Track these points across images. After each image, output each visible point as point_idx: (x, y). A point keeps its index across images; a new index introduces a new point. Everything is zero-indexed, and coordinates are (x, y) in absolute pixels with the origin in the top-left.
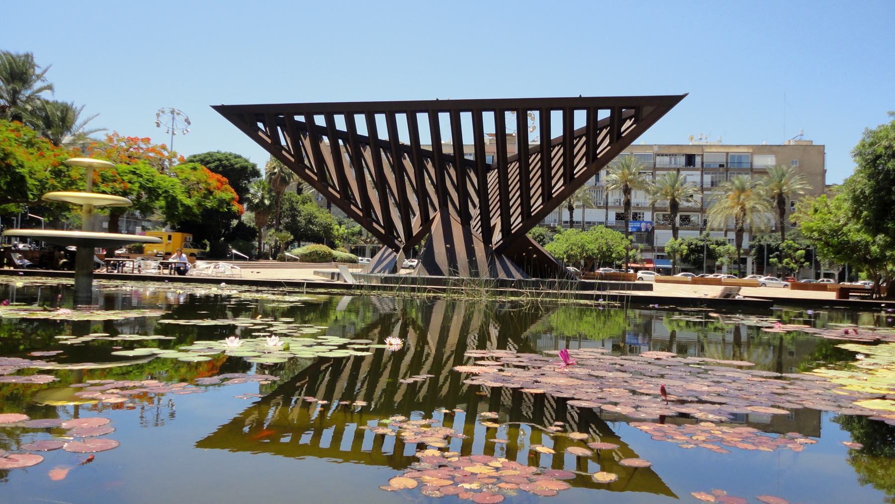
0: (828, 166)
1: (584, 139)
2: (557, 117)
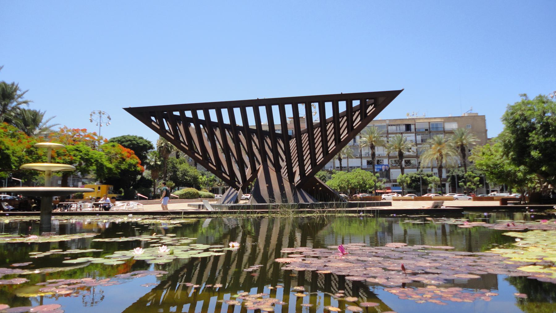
1: (345, 118)
2: (329, 106)
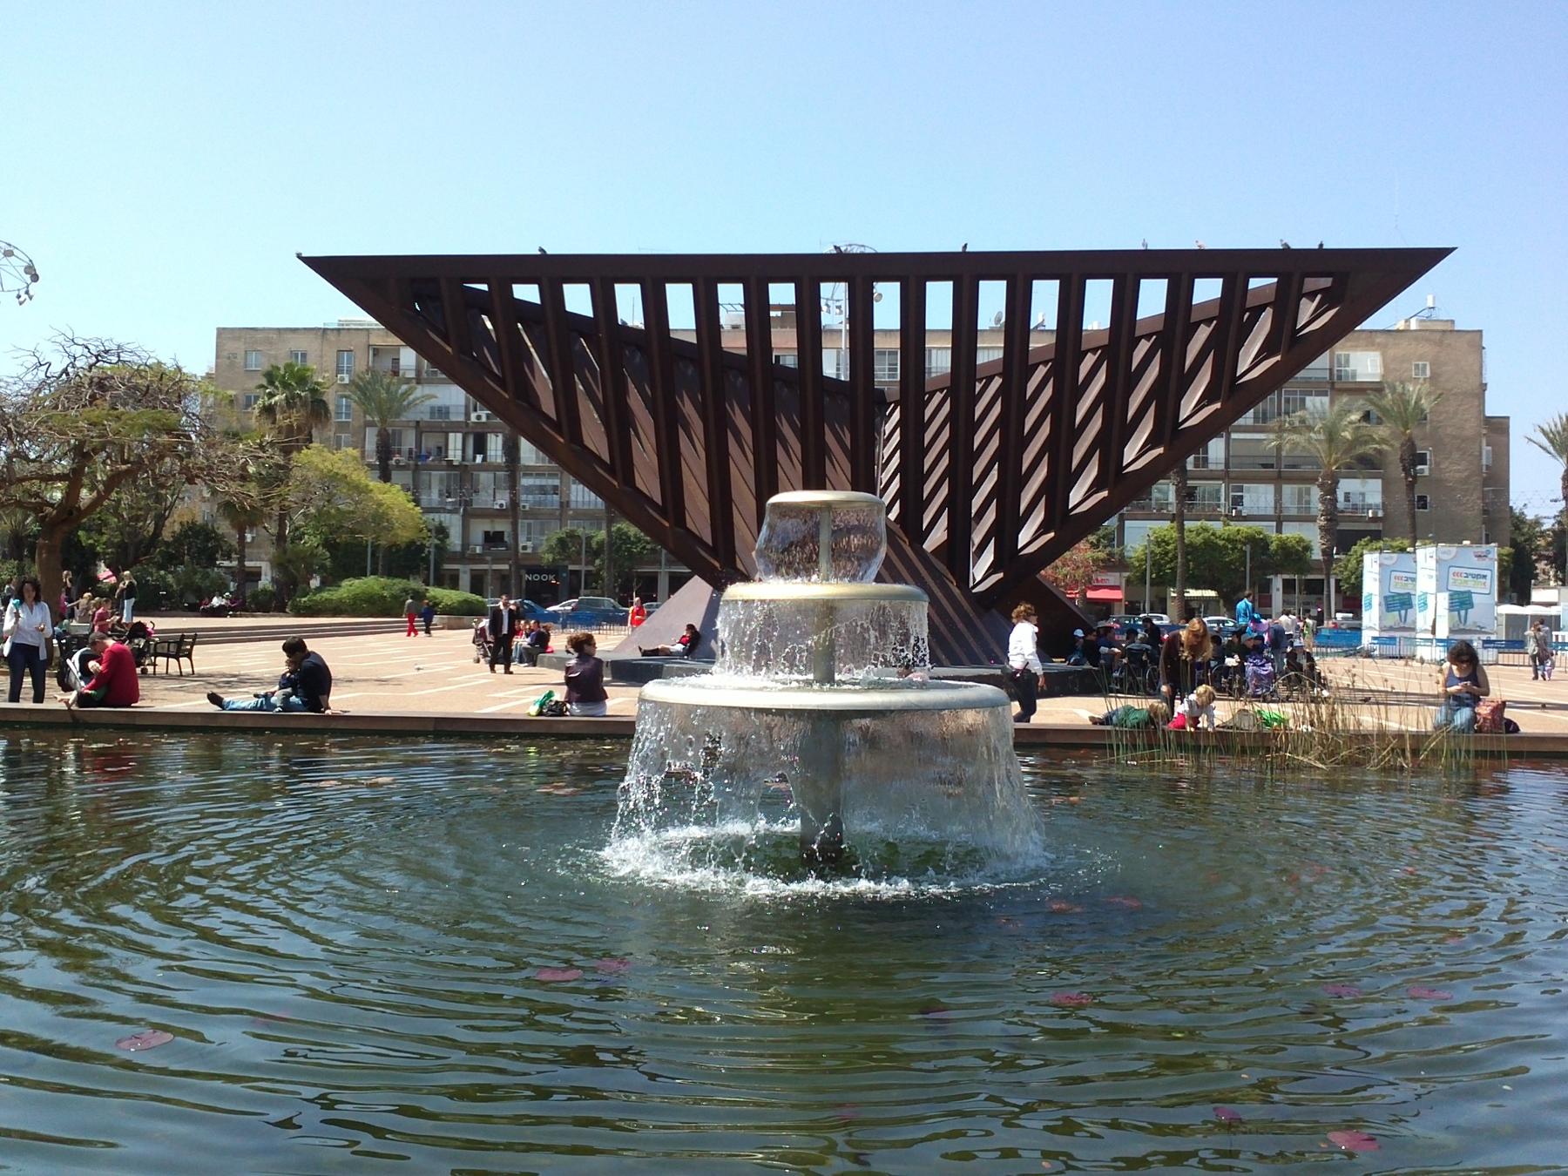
0: (1488, 378)
1: (997, 382)
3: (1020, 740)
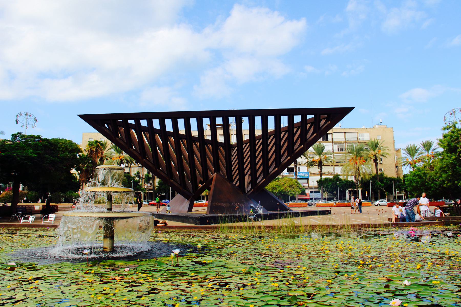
1: (249, 144)
2: (271, 120)
3: (325, 139)
